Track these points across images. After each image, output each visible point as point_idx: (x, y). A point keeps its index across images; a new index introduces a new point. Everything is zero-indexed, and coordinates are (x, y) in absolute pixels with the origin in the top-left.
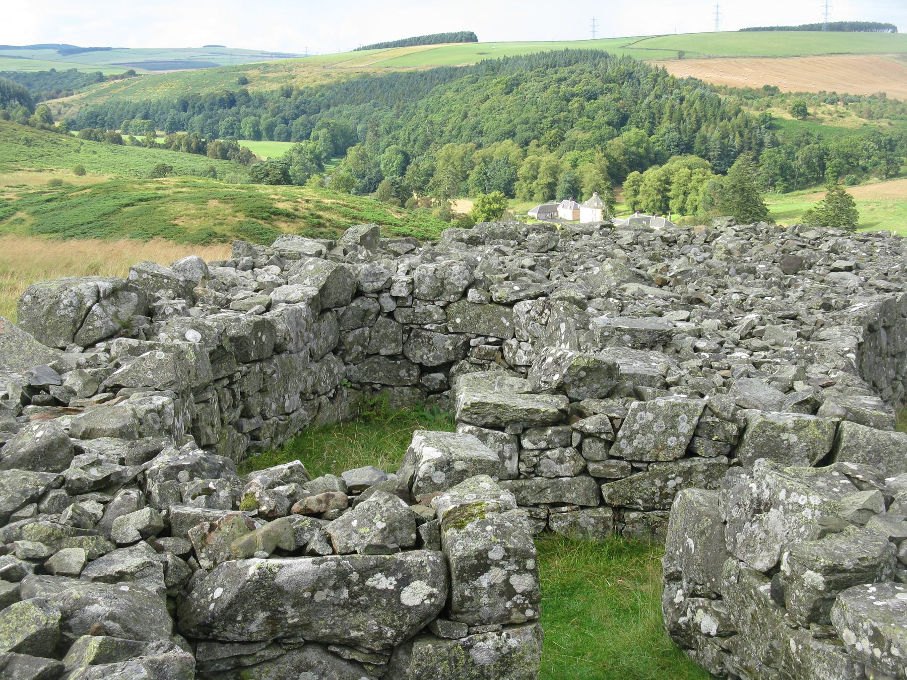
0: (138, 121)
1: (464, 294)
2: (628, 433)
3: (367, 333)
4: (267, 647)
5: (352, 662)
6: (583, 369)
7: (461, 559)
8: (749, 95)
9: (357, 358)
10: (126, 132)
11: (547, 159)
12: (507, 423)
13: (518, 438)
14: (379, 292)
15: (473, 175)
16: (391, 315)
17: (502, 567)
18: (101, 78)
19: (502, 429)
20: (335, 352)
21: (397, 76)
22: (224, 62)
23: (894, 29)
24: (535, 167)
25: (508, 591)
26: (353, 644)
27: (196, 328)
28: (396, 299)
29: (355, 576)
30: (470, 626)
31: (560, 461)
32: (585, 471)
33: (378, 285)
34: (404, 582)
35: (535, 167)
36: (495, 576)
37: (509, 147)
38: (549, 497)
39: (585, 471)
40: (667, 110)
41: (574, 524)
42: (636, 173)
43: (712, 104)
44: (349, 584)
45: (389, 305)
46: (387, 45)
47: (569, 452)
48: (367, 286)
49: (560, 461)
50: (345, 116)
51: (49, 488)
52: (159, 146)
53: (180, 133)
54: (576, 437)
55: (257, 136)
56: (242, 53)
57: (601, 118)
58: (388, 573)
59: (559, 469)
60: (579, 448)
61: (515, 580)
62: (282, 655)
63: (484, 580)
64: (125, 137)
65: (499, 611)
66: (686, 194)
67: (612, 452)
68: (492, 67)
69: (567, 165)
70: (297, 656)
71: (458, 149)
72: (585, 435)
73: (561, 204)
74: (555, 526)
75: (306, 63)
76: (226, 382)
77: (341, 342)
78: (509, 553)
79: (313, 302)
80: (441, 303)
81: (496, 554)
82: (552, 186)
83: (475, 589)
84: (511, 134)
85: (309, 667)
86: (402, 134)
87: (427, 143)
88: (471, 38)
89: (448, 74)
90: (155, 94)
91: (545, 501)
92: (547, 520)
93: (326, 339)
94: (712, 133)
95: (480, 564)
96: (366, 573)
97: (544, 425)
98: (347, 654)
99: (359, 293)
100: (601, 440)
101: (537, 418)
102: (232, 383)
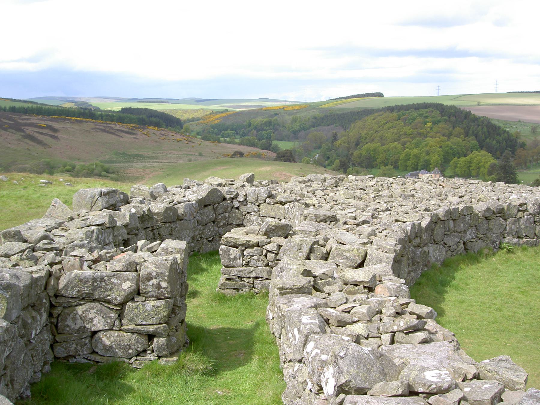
0: (229, 131)
2: (283, 250)
3: (227, 215)
4: (80, 300)
5: (108, 307)
6: (274, 226)
7: (143, 275)
9: (223, 225)
10: (223, 137)
12: (240, 245)
13: (243, 251)
14: (233, 199)
16: (237, 208)
17: (156, 278)
19: (237, 248)
20: (214, 222)
25: (159, 287)
26: (109, 302)
27: (134, 207)
28: (239, 202)
30: (146, 298)
31: (258, 260)
33: (232, 196)
36: (154, 281)
38: (253, 275)
44: (105, 281)
45: (236, 204)
47: (262, 257)
48: (228, 197)
49: (258, 260)
51: (27, 248)
52: (236, 143)
60: (266, 256)
61: (161, 283)
62: (85, 304)
63: (151, 283)
64: (222, 139)
66: (479, 168)
67: (278, 258)
68: (391, 109)
72: (268, 251)
73: (420, 172)
76: (150, 229)
77: (216, 219)
78: (158, 274)
79: (199, 201)
80: (257, 204)
83: (147, 285)
85: (93, 308)
88: (381, 95)
89: (367, 112)
91: (252, 276)
92: (253, 283)
95: (149, 277)
97: (253, 246)
98: (106, 305)
99: (225, 199)
100: (274, 253)
101: (251, 243)
102: (153, 230)
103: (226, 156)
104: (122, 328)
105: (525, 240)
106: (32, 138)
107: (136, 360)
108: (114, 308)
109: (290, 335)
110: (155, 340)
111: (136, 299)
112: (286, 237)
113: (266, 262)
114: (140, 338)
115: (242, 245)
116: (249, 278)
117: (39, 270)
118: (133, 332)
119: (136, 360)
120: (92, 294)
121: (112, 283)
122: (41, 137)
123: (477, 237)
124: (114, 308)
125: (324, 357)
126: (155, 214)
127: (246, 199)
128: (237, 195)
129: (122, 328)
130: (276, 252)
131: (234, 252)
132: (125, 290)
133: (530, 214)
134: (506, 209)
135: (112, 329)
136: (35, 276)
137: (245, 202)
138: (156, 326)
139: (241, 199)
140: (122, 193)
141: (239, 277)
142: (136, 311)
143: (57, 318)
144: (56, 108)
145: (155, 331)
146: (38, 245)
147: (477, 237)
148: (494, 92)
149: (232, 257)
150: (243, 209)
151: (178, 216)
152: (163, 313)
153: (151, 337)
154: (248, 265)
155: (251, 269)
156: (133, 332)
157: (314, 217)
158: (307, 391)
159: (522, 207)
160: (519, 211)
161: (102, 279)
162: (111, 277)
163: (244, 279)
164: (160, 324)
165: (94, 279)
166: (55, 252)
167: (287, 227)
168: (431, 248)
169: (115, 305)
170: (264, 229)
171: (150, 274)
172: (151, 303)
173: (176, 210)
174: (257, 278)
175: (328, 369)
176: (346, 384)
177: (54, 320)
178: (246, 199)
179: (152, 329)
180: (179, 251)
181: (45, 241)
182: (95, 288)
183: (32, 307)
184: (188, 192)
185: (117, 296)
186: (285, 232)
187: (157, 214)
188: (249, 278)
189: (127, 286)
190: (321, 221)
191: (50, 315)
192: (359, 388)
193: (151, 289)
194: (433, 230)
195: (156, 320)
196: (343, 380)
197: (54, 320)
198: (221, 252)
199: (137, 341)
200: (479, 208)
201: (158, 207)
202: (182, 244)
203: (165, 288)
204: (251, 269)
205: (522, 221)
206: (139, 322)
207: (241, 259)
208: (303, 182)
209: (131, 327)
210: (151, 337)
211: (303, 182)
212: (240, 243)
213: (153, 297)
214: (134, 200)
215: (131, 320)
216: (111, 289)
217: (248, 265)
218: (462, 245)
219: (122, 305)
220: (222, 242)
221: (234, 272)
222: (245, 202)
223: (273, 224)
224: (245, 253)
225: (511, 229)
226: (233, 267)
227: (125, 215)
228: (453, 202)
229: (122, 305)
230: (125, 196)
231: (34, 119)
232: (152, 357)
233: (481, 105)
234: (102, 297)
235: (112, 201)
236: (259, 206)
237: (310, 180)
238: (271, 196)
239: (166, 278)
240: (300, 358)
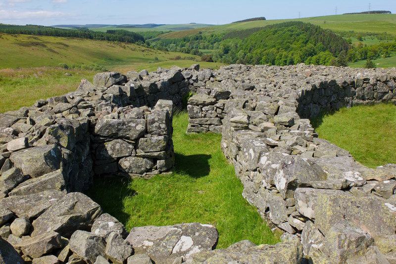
1: (209, 79)
5: (128, 142)
8: (343, 34)
11: (285, 53)
13: (202, 108)
15: (264, 58)
18: (163, 33)
19: (198, 106)
21: (242, 31)
22: (196, 28)
23: (390, 12)
24: (281, 56)
25: (160, 128)
26: (128, 138)
28: (193, 80)
29: (126, 123)
32: (217, 116)
34: (137, 125)
35: (281, 56)
36: (156, 124)
37: (274, 50)
38: (208, 122)
39: (217, 116)
40: (319, 38)
41: (214, 129)
42: (310, 57)
43: (332, 35)
46: (240, 22)
48: (186, 77)
50: (231, 43)
53: (183, 48)
54: (215, 108)
55: (204, 48)
56: (200, 25)
57: (301, 41)
58: (134, 123)
59: (212, 116)
60: (216, 110)
61: (161, 125)
63: (154, 125)
65: (158, 132)
68: (271, 27)
69: (290, 55)
70: (116, 140)
71: (259, 51)
72: (217, 107)
74: (210, 129)
75: (218, 27)
79: (170, 80)
80: (204, 81)
81: (156, 120)
82: (285, 61)
84: (274, 46)
85: (118, 142)
86: (244, 47)
87: (250, 49)
88: (263, 19)
89: (258, 29)
90: (176, 37)
93: (175, 90)
94: (333, 46)
95: (153, 122)
96: (129, 122)
97: (207, 105)
98: (127, 140)
100: (220, 109)
103: (171, 59)
104: (137, 154)
105: (367, 101)
106: (51, 50)
107: (146, 174)
108: (132, 142)
109: (247, 154)
110: (158, 161)
111: (145, 136)
112: (227, 99)
113: (216, 114)
114: (148, 161)
115: (201, 104)
116: (206, 124)
117: (84, 116)
118: (144, 157)
119: (146, 174)
120: (118, 134)
121: (130, 126)
122: (56, 50)
123: (338, 99)
124: (132, 142)
125: (274, 166)
126: (144, 88)
127: (197, 79)
128: (192, 76)
129: (137, 154)
130: (222, 108)
131: (196, 109)
132: (138, 130)
133: (371, 85)
134: (355, 82)
135: (130, 156)
136: (81, 123)
137: (196, 81)
138: (159, 153)
139: (194, 78)
140: (123, 75)
141: (200, 124)
142: (145, 143)
143: (96, 150)
144: (63, 31)
145: (158, 156)
146: (79, 105)
147: (338, 99)
148: (333, 14)
149: (195, 112)
150: (195, 84)
151: (158, 89)
152: (163, 144)
153: (154, 160)
154: (205, 116)
155: (207, 119)
156: (144, 157)
157: (242, 87)
158: (262, 188)
159: (366, 80)
160: (364, 83)
161: (124, 124)
162: (129, 122)
163: (203, 126)
164: (161, 151)
165: (119, 124)
166: (90, 108)
167: (228, 93)
168: (312, 106)
169: (132, 140)
170: (214, 94)
171: (153, 119)
172: (155, 138)
173: (156, 85)
174: (210, 125)
175: (279, 172)
176: (294, 182)
177: (93, 151)
178: (197, 79)
179: (156, 154)
180: (169, 106)
181: (83, 102)
182: (119, 130)
183: (80, 143)
184: (162, 75)
185: (133, 134)
186: (226, 95)
187: (146, 87)
188: (206, 124)
189: (140, 127)
190: (245, 90)
191: (91, 149)
192: (303, 184)
193: (154, 129)
194: (313, 95)
195: (158, 149)
196: (291, 179)
197: (93, 151)
198: (188, 109)
199: (146, 163)
200: (339, 82)
201: (146, 84)
202: (170, 102)
203: (164, 129)
204: (207, 119)
205: (365, 89)
206: (148, 151)
207: (201, 113)
208: (228, 69)
209: (143, 154)
210: (154, 160)
211: (228, 69)
212: (200, 103)
213: (156, 134)
214: (131, 80)
215: (143, 149)
216: (130, 130)
217: (205, 116)
218: (329, 105)
219: (137, 140)
220: (188, 102)
221: (197, 121)
222: (196, 81)
223: (220, 91)
224: (203, 109)
225: (359, 95)
226: (196, 118)
227: (127, 88)
228: (317, 80)
229: (137, 140)
230: (125, 77)
231: (52, 39)
232: (156, 172)
233: (27, 177)
234: (124, 135)
235: (118, 80)
236: (205, 82)
237: (231, 68)
238: (212, 76)
239: (164, 122)
240: (255, 168)
